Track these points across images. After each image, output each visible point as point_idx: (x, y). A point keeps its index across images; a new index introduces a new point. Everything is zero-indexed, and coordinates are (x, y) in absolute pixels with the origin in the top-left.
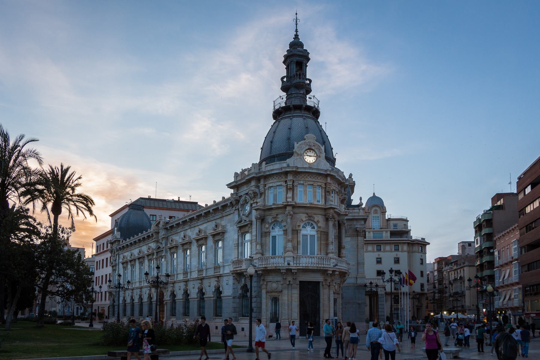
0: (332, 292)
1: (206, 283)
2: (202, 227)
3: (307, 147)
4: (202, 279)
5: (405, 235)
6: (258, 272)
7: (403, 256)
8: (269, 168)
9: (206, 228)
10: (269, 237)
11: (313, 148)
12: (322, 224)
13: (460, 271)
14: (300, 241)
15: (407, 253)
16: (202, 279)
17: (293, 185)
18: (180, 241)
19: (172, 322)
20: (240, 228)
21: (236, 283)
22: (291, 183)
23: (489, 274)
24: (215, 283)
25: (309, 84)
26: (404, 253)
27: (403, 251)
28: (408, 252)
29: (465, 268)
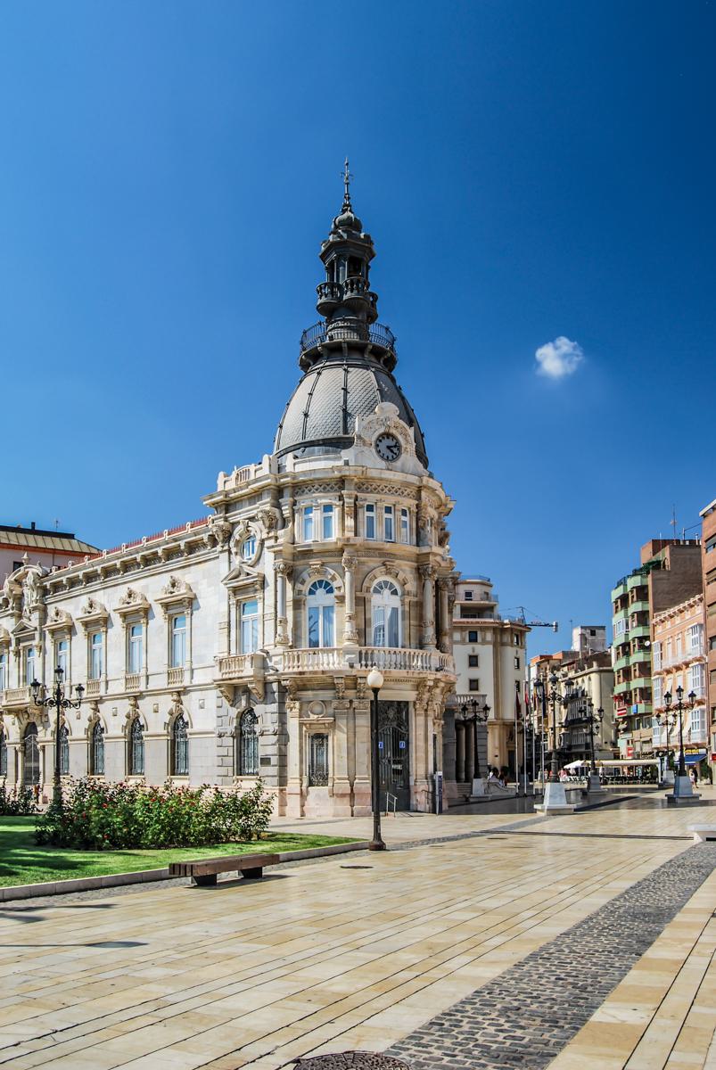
0: (430, 723)
1: (145, 705)
2: (135, 586)
3: (382, 430)
4: (180, 693)
5: (488, 613)
6: (283, 683)
7: (485, 652)
8: (300, 468)
9: (146, 587)
10: (304, 609)
11: (393, 431)
12: (412, 586)
13: (583, 681)
14: (403, 619)
15: (491, 647)
16: (180, 693)
17: (355, 504)
18: (80, 614)
19: (431, 790)
20: (236, 591)
21: (226, 703)
22: (352, 501)
23: (642, 686)
24: (172, 705)
25: (373, 304)
26: (486, 646)
27: (484, 642)
28: (495, 646)
29: (593, 676)
